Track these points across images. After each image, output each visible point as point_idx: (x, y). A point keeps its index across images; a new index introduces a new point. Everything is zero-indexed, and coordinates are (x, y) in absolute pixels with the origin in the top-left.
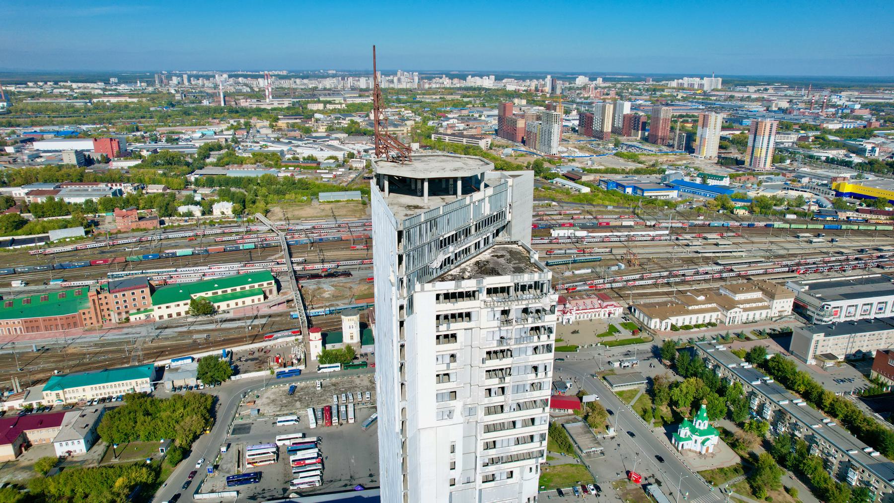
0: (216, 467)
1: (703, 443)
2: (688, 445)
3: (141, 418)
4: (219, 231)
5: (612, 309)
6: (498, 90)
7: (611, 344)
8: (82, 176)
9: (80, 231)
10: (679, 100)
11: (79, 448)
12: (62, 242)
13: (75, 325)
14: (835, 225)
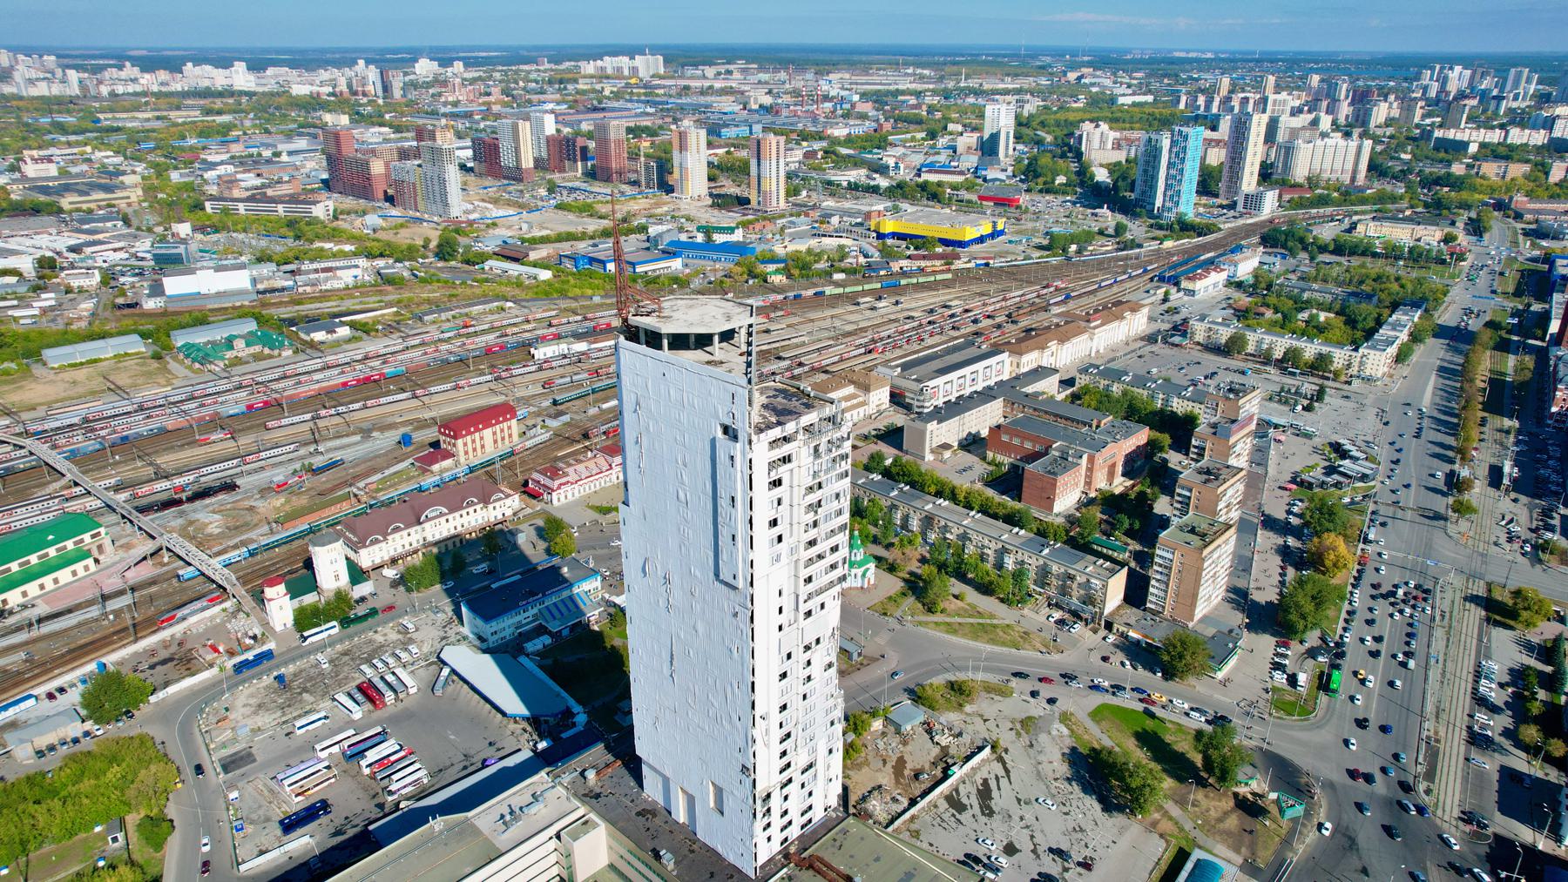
10: (609, 98)
14: (892, 281)
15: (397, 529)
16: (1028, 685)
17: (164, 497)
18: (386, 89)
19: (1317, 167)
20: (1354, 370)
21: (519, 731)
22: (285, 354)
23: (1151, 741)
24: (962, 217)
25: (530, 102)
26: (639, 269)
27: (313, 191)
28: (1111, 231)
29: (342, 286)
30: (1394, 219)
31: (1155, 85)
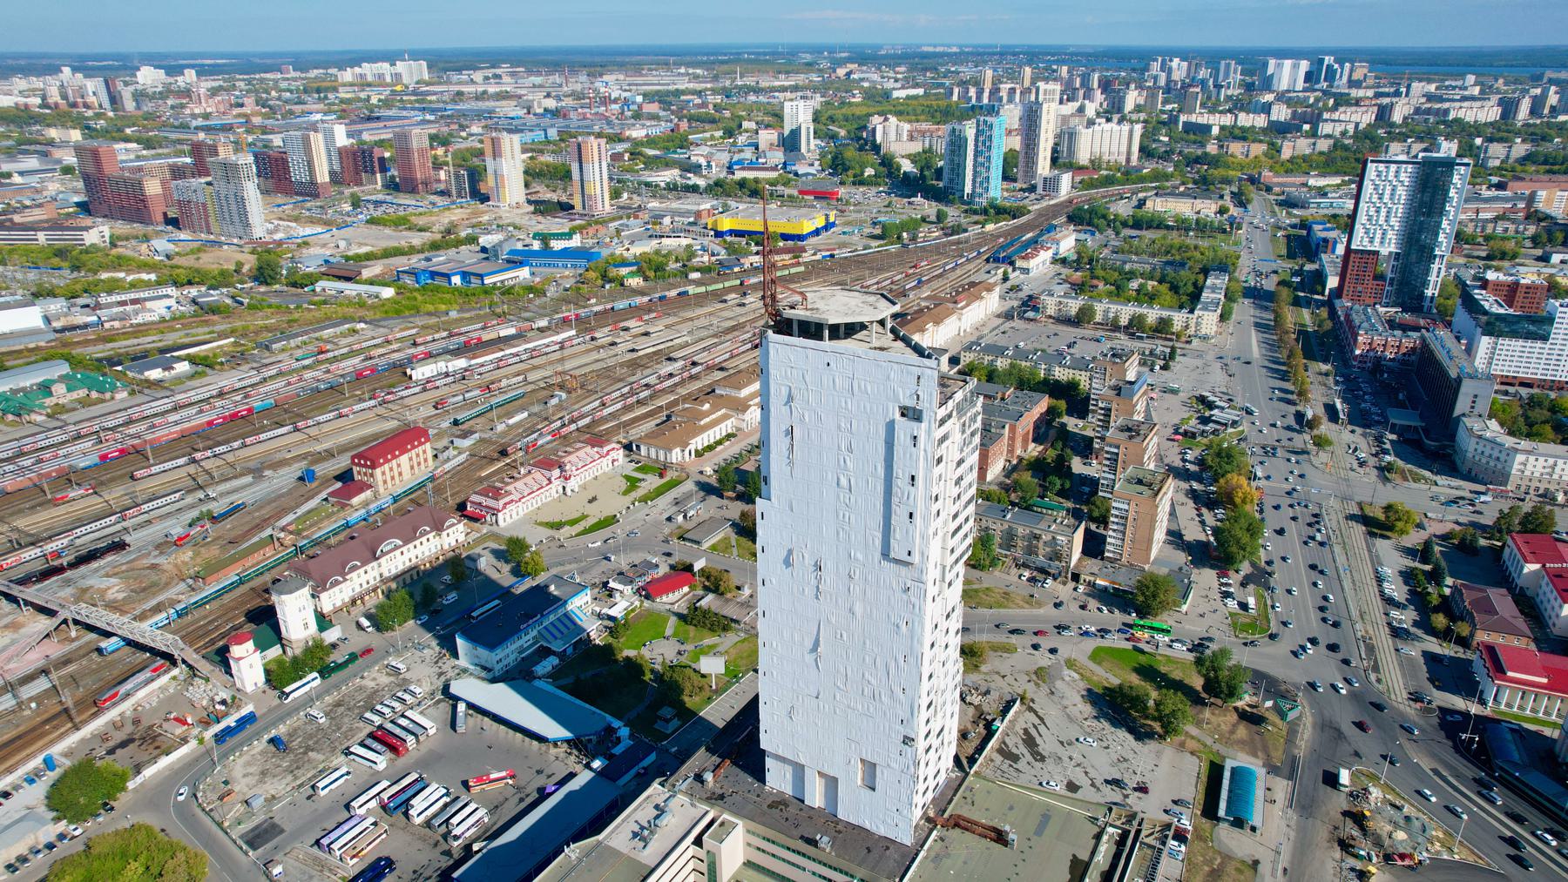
15: (354, 568)
16: (1029, 640)
17: (39, 566)
18: (114, 100)
19: (1097, 150)
20: (1191, 331)
21: (562, 755)
22: (119, 396)
23: (1148, 672)
24: (794, 212)
25: (291, 112)
26: (488, 281)
27: (69, 214)
28: (933, 218)
29: (156, 318)
30: (1172, 194)
31: (920, 79)
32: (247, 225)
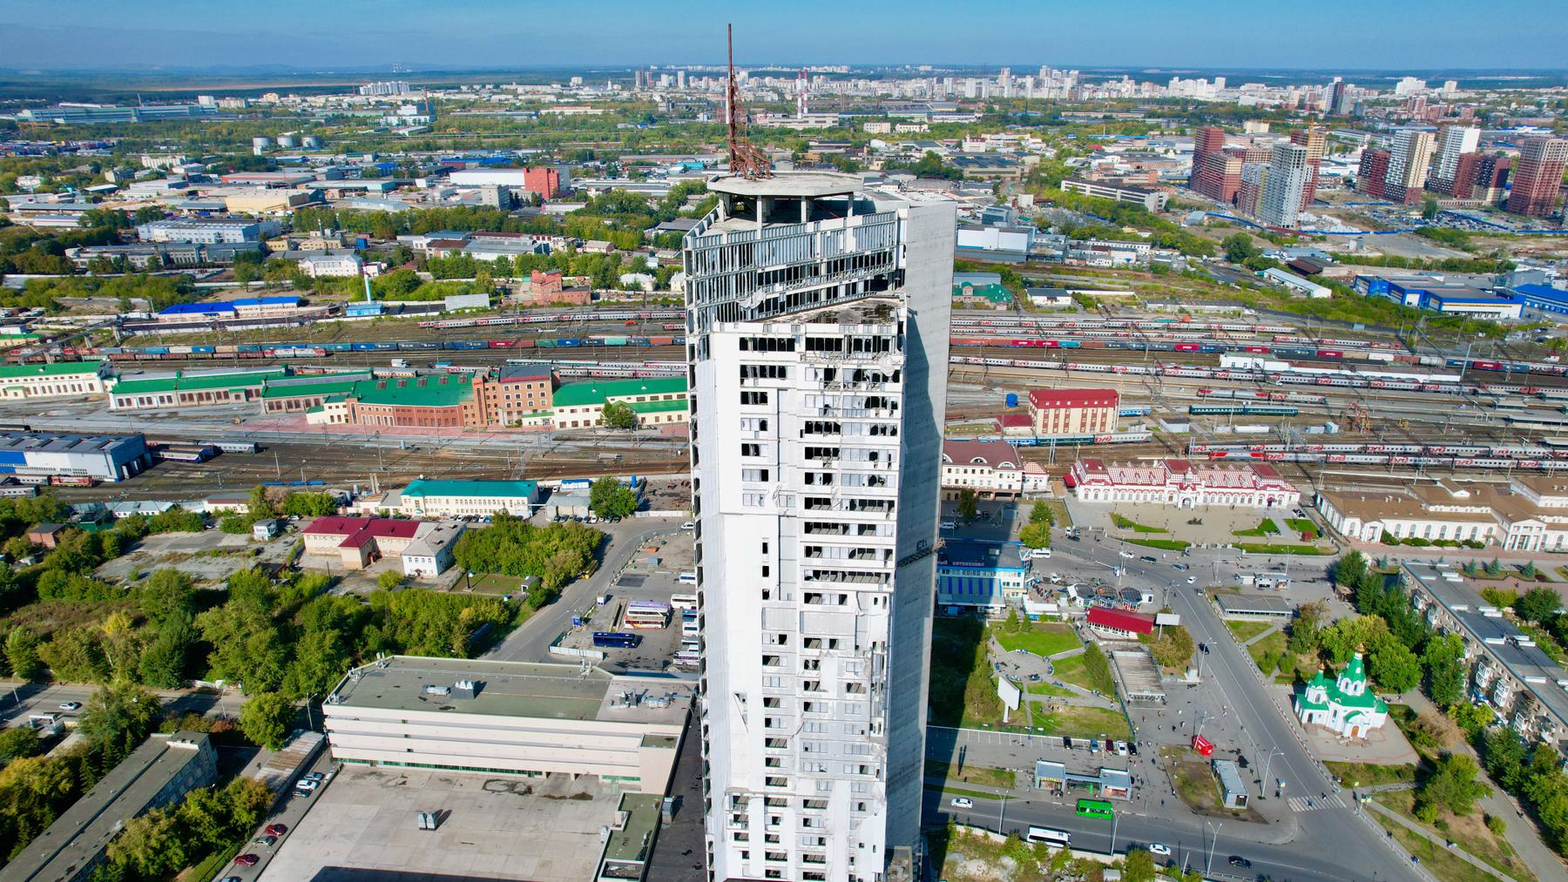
0: (587, 621)
1: (1347, 719)
2: (1322, 718)
3: (505, 543)
4: (672, 315)
5: (1276, 493)
6: (1222, 105)
7: (1253, 549)
8: (501, 223)
9: (483, 300)
11: (429, 568)
12: (460, 314)
13: (454, 422)
32: (1280, 211)
